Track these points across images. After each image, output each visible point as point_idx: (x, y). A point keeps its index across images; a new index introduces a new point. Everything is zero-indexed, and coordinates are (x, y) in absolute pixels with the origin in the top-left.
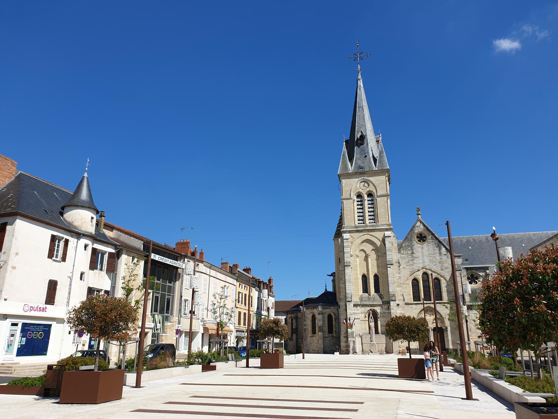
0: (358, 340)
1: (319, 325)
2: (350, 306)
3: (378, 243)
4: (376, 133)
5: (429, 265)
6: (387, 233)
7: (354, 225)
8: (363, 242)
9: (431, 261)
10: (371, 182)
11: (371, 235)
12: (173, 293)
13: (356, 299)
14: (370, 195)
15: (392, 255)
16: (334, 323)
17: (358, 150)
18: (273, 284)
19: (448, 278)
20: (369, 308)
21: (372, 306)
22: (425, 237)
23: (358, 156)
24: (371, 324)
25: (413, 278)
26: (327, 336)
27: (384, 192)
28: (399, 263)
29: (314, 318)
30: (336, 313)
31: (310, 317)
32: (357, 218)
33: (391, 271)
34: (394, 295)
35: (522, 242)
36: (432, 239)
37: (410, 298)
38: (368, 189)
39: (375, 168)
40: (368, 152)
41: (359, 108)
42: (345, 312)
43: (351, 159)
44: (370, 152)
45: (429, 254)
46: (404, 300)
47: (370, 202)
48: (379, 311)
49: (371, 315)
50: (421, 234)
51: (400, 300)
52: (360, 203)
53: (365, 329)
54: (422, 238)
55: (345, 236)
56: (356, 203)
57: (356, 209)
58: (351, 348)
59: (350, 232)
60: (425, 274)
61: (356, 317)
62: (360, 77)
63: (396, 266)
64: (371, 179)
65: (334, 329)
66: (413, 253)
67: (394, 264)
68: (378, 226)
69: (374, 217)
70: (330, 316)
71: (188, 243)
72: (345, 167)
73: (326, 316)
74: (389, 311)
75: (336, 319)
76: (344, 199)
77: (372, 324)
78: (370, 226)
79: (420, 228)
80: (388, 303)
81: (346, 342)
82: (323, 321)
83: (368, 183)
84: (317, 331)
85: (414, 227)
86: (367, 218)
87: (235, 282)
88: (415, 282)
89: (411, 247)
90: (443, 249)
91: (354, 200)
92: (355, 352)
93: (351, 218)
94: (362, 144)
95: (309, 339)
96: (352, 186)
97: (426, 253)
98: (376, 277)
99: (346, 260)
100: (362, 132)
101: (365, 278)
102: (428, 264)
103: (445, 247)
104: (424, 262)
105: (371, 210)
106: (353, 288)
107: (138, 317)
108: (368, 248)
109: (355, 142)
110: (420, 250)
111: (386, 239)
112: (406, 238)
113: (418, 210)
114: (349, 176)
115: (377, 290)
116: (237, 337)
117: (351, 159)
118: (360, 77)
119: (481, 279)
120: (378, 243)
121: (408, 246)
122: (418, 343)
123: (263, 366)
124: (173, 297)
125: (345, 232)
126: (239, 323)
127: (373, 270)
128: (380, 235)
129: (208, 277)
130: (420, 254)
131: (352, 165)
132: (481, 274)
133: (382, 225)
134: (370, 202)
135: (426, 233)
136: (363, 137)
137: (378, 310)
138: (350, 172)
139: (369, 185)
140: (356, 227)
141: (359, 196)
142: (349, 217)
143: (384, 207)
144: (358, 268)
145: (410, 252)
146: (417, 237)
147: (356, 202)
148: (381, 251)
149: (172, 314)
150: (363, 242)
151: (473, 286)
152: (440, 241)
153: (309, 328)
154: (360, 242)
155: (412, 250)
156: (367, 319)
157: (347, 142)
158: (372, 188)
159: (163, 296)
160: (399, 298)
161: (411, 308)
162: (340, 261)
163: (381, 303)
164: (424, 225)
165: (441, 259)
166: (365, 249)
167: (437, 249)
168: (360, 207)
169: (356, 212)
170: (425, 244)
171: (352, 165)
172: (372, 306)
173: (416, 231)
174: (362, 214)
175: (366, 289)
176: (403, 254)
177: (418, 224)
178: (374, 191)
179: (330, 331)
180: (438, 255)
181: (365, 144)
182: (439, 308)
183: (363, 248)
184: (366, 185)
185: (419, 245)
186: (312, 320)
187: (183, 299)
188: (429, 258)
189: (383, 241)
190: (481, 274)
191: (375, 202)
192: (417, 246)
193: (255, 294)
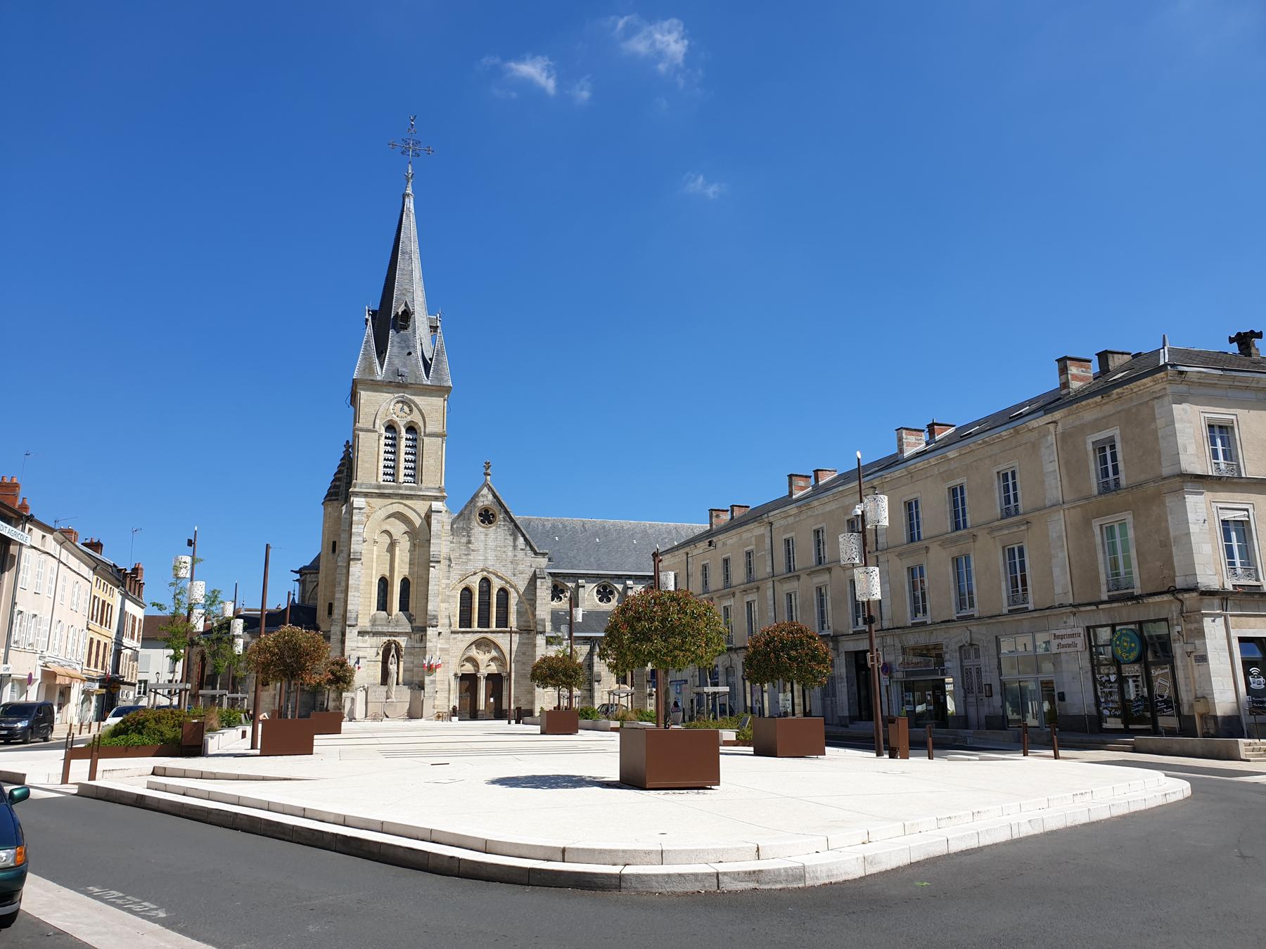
0: (360, 696)
2: (351, 634)
3: (418, 522)
4: (431, 309)
6: (436, 505)
7: (374, 482)
8: (389, 517)
9: (498, 558)
10: (417, 406)
13: (364, 623)
14: (411, 429)
15: (441, 545)
17: (397, 339)
18: (144, 578)
19: (522, 590)
20: (385, 639)
21: (392, 634)
22: (494, 516)
23: (396, 350)
27: (438, 429)
32: (381, 470)
33: (436, 574)
34: (435, 617)
35: (632, 537)
38: (409, 418)
39: (426, 382)
40: (415, 347)
41: (403, 253)
43: (381, 352)
44: (419, 347)
47: (410, 443)
48: (403, 644)
49: (393, 652)
50: (486, 511)
51: (443, 625)
52: (390, 442)
53: (375, 678)
54: (487, 517)
55: (358, 502)
56: (383, 441)
57: (382, 453)
58: (346, 710)
59: (366, 495)
60: (486, 582)
61: (361, 654)
62: (409, 191)
63: (444, 562)
64: (416, 399)
66: (469, 542)
68: (421, 490)
69: (416, 472)
71: (16, 485)
72: (369, 368)
76: (362, 430)
78: (407, 488)
79: (486, 499)
80: (422, 630)
83: (409, 407)
85: (476, 495)
86: (402, 472)
87: (93, 578)
88: (467, 593)
89: (468, 531)
90: (521, 539)
91: (380, 435)
92: (352, 719)
93: (370, 468)
94: (405, 328)
96: (379, 406)
97: (491, 544)
98: (405, 583)
99: (354, 547)
100: (406, 305)
101: (384, 584)
102: (492, 564)
103: (523, 535)
104: (486, 559)
105: (410, 457)
106: (361, 600)
108: (398, 528)
109: (389, 321)
110: (482, 537)
111: (434, 516)
112: (461, 514)
113: (488, 465)
114: (375, 386)
115: (404, 606)
116: (84, 692)
117: (381, 352)
118: (409, 191)
119: (568, 594)
120: (418, 522)
125: (357, 494)
126: (89, 665)
127: (402, 569)
128: (422, 507)
129: (56, 562)
130: (482, 545)
131: (382, 367)
132: (569, 585)
133: (428, 489)
134: (410, 443)
135: (495, 509)
136: (407, 315)
137: (403, 641)
138: (379, 378)
139: (411, 410)
140: (379, 487)
141: (391, 427)
143: (434, 452)
145: (464, 540)
146: (480, 515)
148: (420, 537)
150: (389, 517)
151: (555, 604)
152: (516, 526)
154: (383, 516)
156: (380, 658)
157: (374, 314)
160: (443, 621)
162: (338, 546)
163: (409, 629)
164: (495, 496)
166: (392, 531)
167: (511, 538)
168: (389, 448)
169: (381, 458)
170: (493, 528)
171: (382, 367)
172: (392, 634)
173: (480, 504)
174: (392, 464)
175: (383, 605)
177: (485, 491)
178: (421, 424)
181: (410, 329)
182: (502, 640)
184: (406, 409)
187: (17, 608)
188: (494, 555)
189: (428, 518)
190: (569, 585)
191: (418, 443)
192: (478, 530)
193: (115, 599)
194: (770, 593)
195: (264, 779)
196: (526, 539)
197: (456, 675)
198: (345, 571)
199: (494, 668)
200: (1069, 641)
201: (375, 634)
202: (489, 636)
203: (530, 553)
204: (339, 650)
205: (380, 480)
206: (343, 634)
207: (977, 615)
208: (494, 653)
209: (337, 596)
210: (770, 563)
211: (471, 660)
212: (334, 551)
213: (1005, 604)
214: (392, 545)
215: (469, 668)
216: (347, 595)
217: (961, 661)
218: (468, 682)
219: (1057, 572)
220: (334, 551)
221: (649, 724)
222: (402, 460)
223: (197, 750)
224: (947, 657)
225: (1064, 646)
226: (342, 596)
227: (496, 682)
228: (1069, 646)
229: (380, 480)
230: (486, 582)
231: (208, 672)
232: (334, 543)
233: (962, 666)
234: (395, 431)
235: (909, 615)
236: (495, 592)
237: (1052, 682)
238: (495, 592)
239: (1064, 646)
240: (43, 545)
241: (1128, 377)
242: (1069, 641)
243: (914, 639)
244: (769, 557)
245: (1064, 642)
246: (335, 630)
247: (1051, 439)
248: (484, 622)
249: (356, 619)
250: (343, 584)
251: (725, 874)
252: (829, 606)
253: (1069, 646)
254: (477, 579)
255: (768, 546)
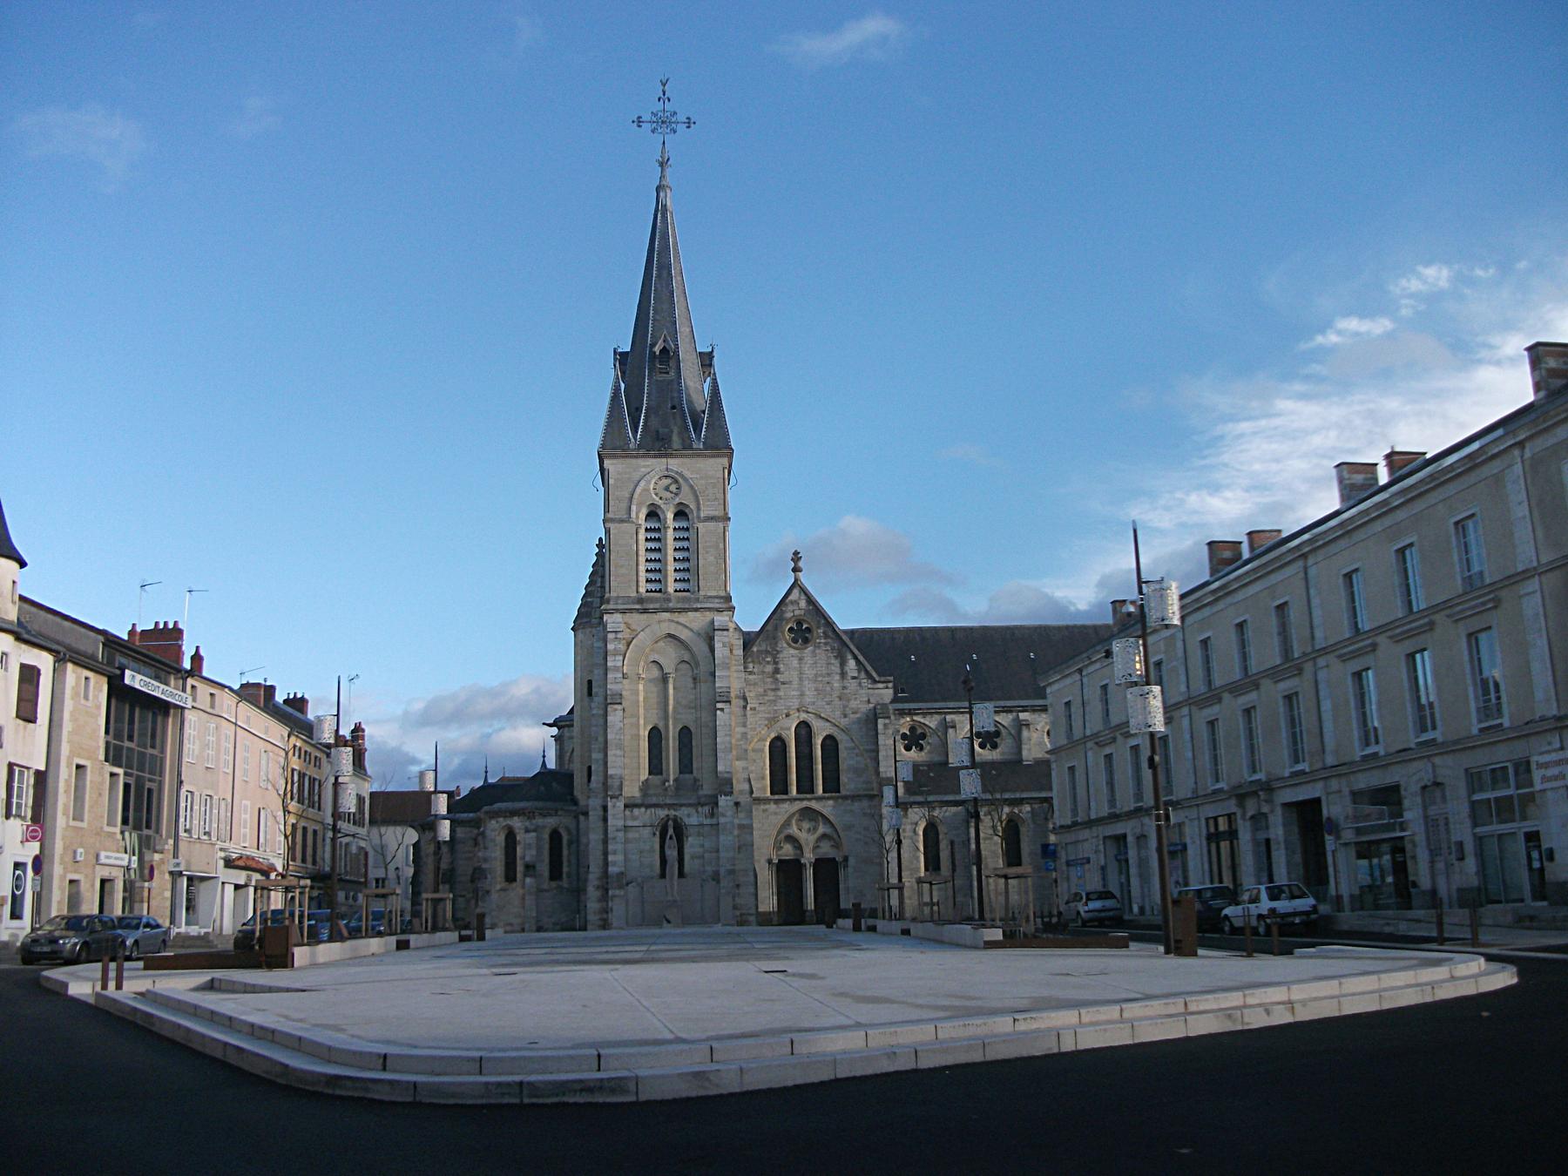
1: (527, 859)
2: (616, 808)
12: (161, 774)
16: (565, 852)
20: (662, 813)
21: (670, 806)
24: (668, 852)
25: (773, 735)
26: (545, 886)
28: (745, 699)
29: (511, 837)
30: (573, 826)
31: (501, 839)
33: (725, 717)
36: (826, 636)
37: (763, 787)
38: (677, 500)
42: (601, 824)
46: (752, 792)
49: (671, 831)
51: (741, 792)
55: (613, 621)
56: (642, 535)
57: (642, 551)
60: (804, 727)
65: (565, 869)
66: (777, 671)
67: (734, 701)
68: (697, 600)
70: (555, 836)
73: (546, 836)
74: (714, 821)
75: (570, 843)
77: (672, 853)
81: (600, 901)
82: (539, 849)
84: (519, 876)
88: (778, 746)
89: (775, 655)
90: (852, 663)
95: (494, 896)
97: (809, 672)
98: (685, 734)
101: (656, 736)
104: (802, 695)
107: (625, 688)
110: (795, 663)
111: (718, 637)
121: (767, 652)
123: (146, 968)
124: (161, 784)
140: (640, 600)
142: (623, 571)
144: (642, 711)
145: (769, 668)
147: (642, 531)
149: (158, 831)
153: (498, 867)
155: (776, 663)
158: (686, 497)
159: (140, 783)
165: (844, 688)
167: (836, 663)
179: (556, 874)
183: (656, 657)
184: (673, 488)
185: (792, 651)
186: (507, 847)
192: (789, 654)
194: (1186, 722)
195: (288, 990)
196: (858, 662)
198: (601, 721)
199: (826, 850)
200: (1555, 771)
201: (648, 806)
202: (814, 805)
204: (600, 831)
205: (642, 590)
206: (605, 808)
207: (1440, 740)
208: (822, 829)
209: (595, 756)
210: (1183, 678)
211: (790, 839)
212: (590, 694)
213: (1474, 720)
214: (664, 679)
215: (788, 851)
216: (606, 755)
217: (1425, 808)
218: (788, 872)
219: (1536, 667)
220: (590, 694)
222: (670, 559)
223: (285, 961)
224: (1406, 803)
225: (1550, 779)
226: (601, 756)
227: (828, 870)
228: (1556, 778)
229: (642, 590)
230: (804, 730)
231: (444, 865)
232: (590, 682)
233: (1426, 817)
234: (659, 520)
235: (1357, 744)
236: (818, 742)
237: (1537, 832)
238: (818, 742)
239: (1550, 779)
240: (212, 707)
241: (730, 456)
242: (1555, 771)
243: (1364, 781)
244: (1182, 670)
245: (1550, 772)
246: (594, 803)
247: (1518, 468)
248: (806, 786)
249: (621, 788)
250: (601, 739)
251: (489, 1059)
252: (1259, 740)
253: (1556, 778)
255: (1180, 653)
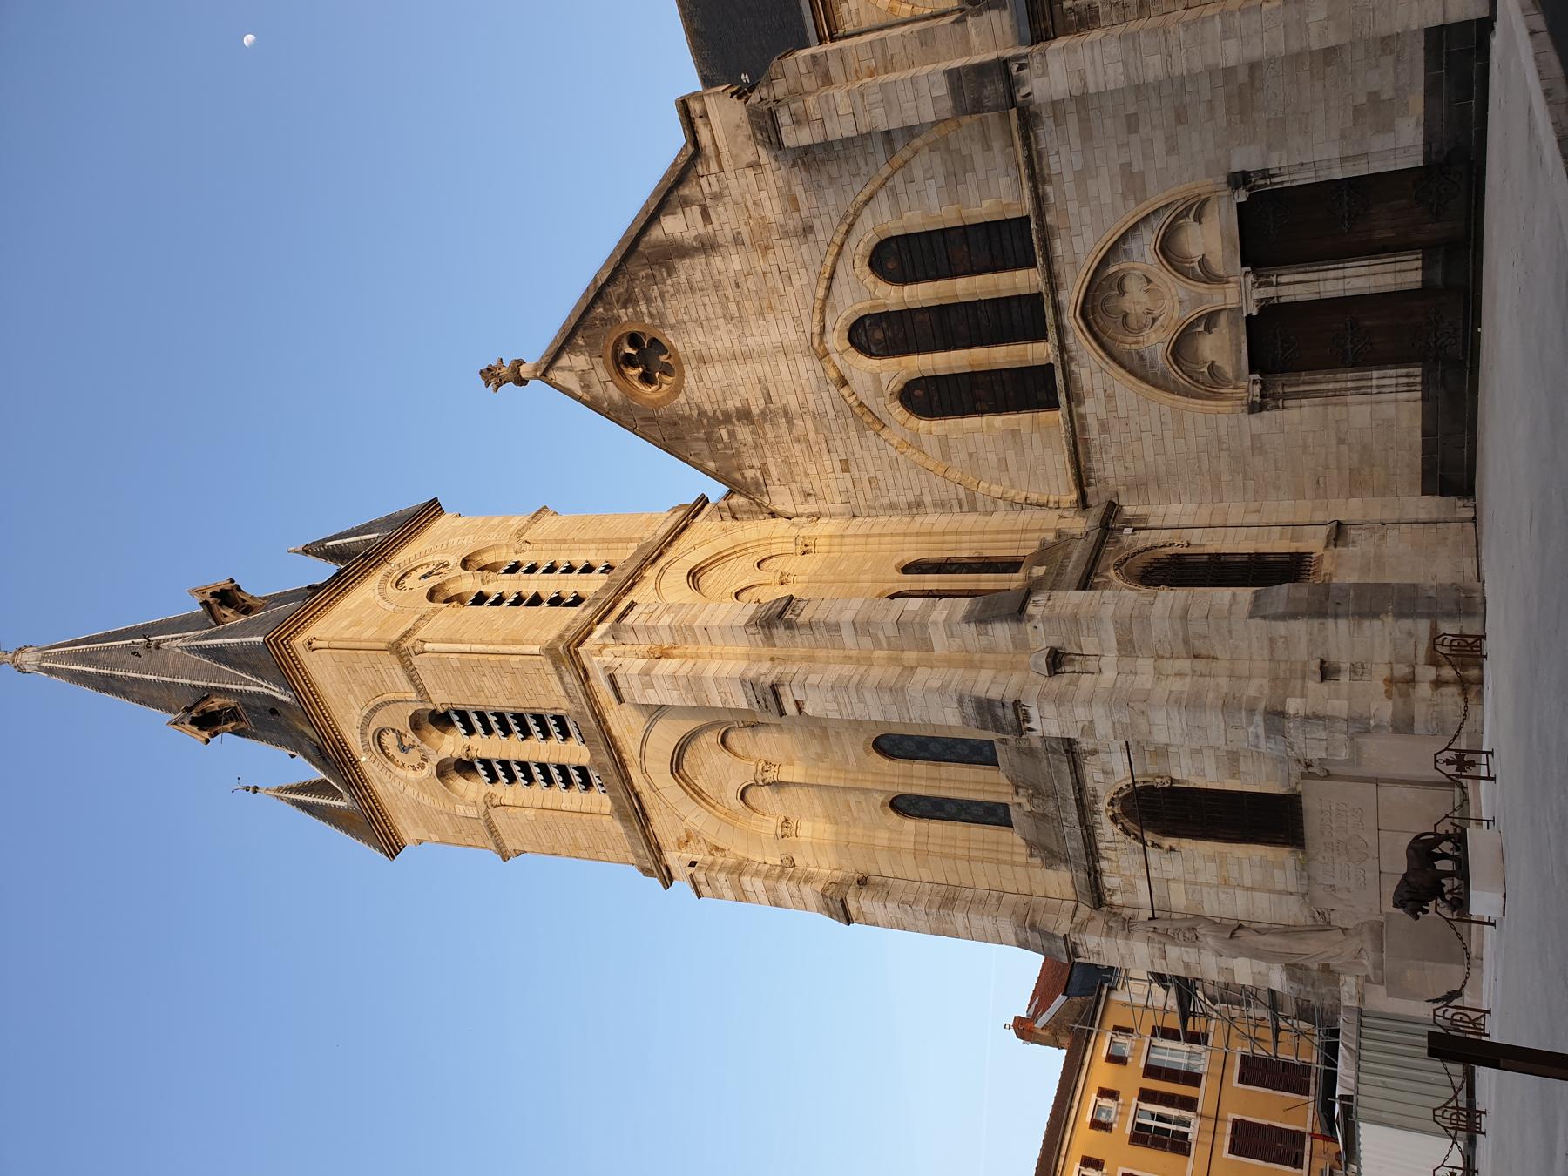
5: (797, 320)
8: (698, 794)
11: (642, 754)
20: (1107, 830)
21: (1084, 808)
45: (729, 318)
66: (745, 415)
88: (925, 398)
90: (673, 226)
97: (723, 339)
110: (714, 373)
122: (1415, 160)
130: (739, 371)
145: (744, 433)
150: (698, 794)
155: (727, 418)
161: (1104, 427)
165: (738, 241)
167: (683, 266)
176: (765, 471)
180: (717, 261)
185: (690, 380)
197: (1254, 408)
202: (1071, 295)
203: (706, 182)
221: (1367, 323)
248: (1021, 317)
254: (863, 368)
